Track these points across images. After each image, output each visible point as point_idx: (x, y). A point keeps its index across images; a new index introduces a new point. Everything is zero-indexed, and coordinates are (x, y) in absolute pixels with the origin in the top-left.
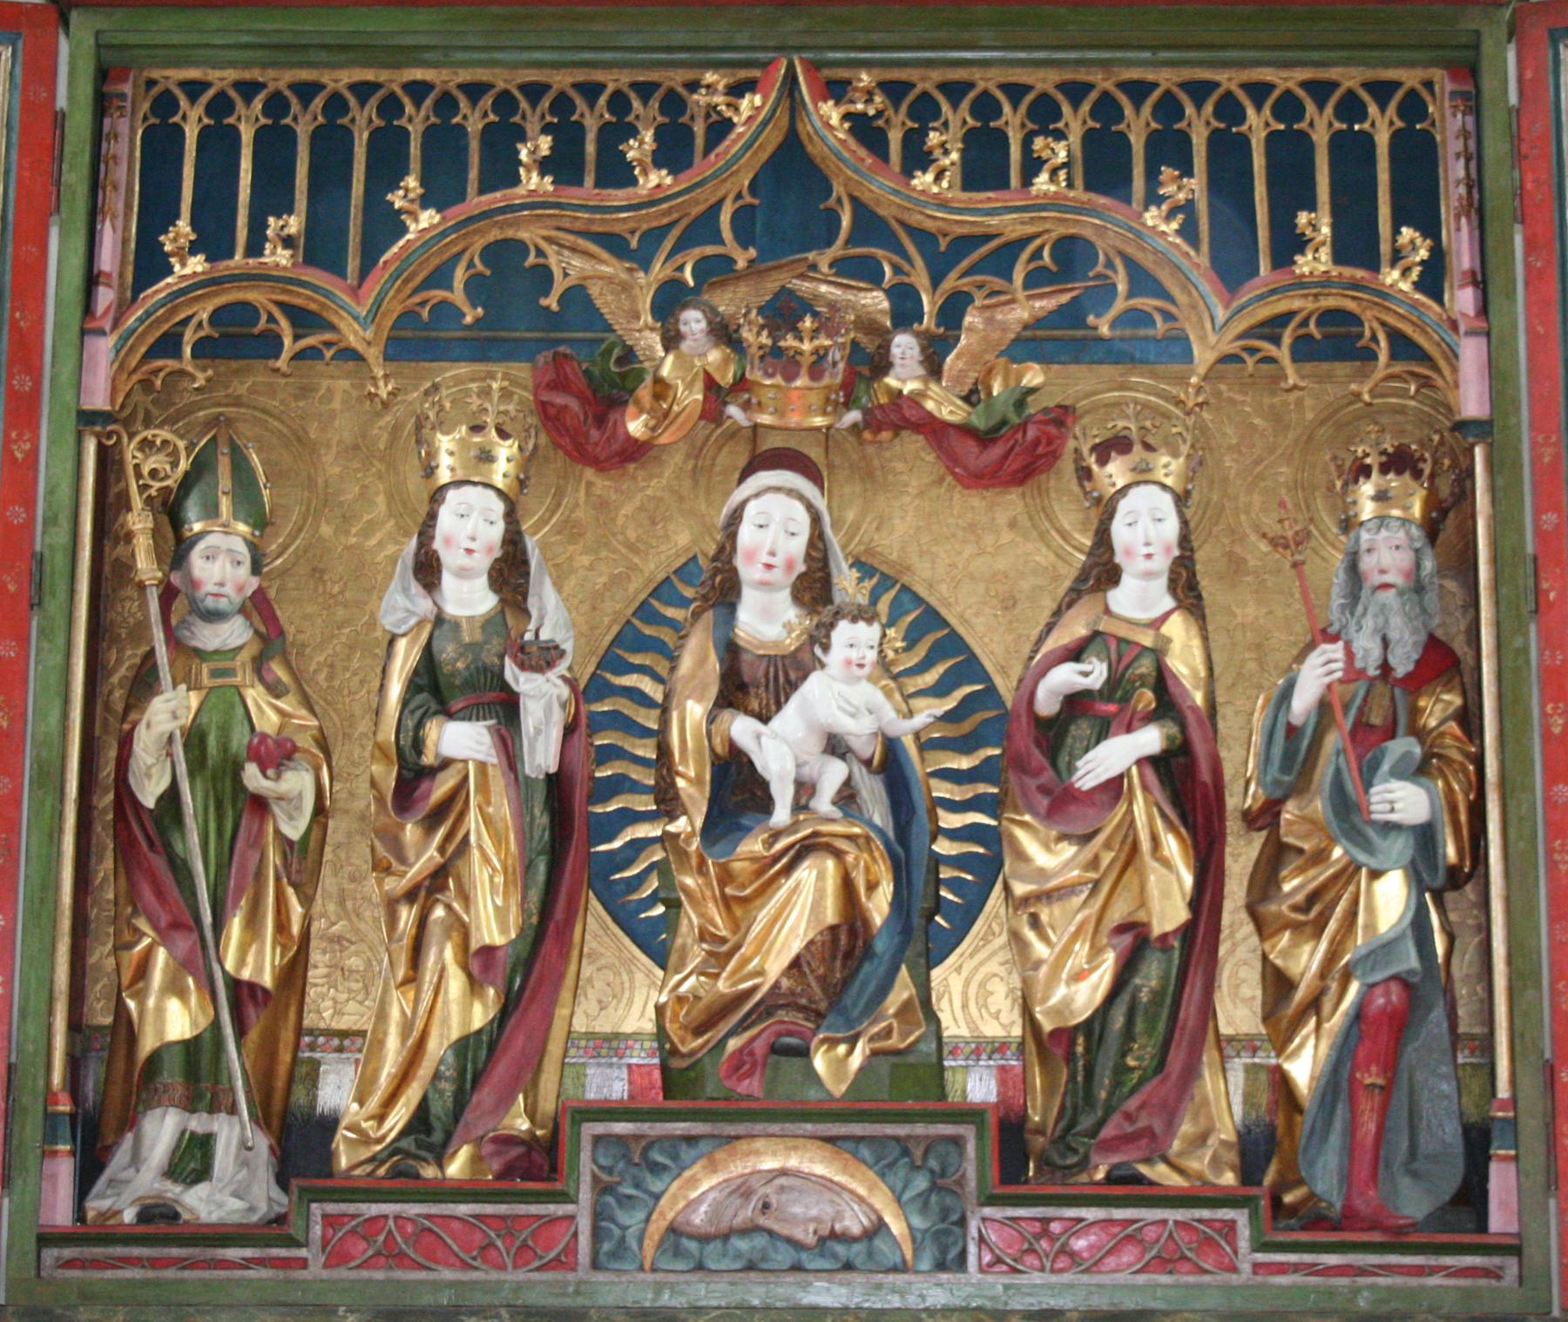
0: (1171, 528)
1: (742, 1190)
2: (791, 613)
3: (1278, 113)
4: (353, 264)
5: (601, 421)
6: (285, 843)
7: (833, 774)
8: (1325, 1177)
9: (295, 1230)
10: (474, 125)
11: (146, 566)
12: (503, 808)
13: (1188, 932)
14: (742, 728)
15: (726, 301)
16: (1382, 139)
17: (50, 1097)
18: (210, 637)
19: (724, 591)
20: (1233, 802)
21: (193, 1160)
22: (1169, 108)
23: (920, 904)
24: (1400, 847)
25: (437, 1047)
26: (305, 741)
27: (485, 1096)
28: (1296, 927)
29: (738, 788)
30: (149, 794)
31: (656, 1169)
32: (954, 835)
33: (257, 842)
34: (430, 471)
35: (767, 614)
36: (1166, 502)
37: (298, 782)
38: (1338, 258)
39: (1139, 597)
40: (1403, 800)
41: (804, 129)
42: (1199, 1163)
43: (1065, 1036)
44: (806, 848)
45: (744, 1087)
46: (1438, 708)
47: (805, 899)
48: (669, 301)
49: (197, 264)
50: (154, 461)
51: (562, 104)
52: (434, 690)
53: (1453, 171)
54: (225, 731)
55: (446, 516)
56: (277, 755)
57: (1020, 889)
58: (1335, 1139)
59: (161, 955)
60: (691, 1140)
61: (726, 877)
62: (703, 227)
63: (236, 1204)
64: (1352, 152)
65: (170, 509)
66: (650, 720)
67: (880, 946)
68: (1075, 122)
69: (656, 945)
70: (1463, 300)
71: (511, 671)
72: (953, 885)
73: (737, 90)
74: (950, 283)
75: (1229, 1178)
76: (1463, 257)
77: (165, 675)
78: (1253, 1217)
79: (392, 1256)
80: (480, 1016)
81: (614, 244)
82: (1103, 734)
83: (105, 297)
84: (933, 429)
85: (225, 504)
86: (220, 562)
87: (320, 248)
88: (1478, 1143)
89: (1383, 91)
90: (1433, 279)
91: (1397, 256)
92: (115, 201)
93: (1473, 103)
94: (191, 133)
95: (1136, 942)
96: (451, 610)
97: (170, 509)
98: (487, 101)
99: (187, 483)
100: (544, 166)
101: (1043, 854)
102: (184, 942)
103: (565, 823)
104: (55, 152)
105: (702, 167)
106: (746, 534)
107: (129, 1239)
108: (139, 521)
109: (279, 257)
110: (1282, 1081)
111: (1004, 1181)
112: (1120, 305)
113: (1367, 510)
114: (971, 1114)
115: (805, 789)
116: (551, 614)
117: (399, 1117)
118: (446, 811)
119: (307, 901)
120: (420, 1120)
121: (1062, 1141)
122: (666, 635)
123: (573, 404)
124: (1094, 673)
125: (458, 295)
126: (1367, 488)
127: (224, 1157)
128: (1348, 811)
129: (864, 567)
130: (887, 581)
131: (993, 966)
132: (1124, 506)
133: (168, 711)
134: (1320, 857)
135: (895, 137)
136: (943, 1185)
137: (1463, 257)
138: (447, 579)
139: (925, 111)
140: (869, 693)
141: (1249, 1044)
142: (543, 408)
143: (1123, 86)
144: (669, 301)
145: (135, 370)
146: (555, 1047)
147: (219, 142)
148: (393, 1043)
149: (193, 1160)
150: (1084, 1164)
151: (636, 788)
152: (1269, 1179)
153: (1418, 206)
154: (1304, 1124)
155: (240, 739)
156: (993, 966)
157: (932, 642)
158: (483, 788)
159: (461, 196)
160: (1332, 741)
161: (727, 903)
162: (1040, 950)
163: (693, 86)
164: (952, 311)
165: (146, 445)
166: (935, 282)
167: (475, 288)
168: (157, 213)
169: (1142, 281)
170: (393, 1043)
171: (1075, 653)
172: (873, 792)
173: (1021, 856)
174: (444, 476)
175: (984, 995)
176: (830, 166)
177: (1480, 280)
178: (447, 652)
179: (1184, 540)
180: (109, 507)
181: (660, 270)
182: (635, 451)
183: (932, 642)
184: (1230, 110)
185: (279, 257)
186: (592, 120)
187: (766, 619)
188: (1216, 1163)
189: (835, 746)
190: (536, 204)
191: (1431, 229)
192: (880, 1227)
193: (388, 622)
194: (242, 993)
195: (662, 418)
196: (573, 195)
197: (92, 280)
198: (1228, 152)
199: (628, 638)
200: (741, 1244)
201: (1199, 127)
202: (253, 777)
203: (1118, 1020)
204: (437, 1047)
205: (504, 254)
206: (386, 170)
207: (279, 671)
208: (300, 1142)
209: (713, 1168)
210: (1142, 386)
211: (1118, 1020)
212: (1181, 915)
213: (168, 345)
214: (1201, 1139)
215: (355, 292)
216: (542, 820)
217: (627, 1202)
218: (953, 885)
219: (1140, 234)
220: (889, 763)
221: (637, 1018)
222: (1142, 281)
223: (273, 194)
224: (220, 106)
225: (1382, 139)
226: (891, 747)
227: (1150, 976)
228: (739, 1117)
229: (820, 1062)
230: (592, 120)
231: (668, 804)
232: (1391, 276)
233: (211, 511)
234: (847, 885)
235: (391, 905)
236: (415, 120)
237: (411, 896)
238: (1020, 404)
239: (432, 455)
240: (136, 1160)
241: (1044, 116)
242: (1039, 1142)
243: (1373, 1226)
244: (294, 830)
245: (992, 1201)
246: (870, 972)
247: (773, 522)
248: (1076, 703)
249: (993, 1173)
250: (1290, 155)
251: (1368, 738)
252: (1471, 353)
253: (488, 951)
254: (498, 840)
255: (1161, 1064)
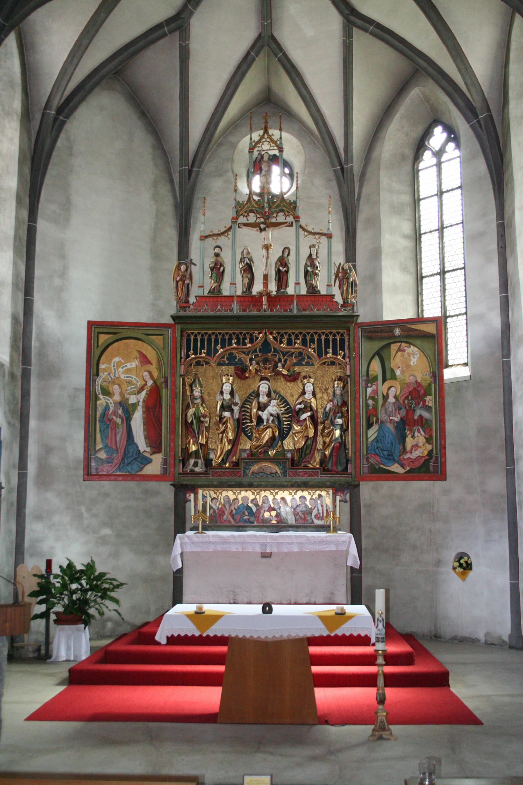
0: (312, 388)
1: (261, 468)
2: (266, 398)
3: (326, 336)
4: (212, 356)
5: (243, 374)
6: (206, 427)
7: (271, 418)
8: (329, 466)
9: (208, 472)
10: (227, 338)
11: (188, 393)
12: (232, 422)
13: (314, 437)
14: (260, 413)
15: (257, 359)
16: (338, 339)
17: (179, 457)
18: (196, 401)
19: (258, 395)
20: (319, 420)
21: (196, 464)
22: (312, 336)
23: (282, 433)
24: (339, 427)
25: (224, 451)
26: (208, 414)
27: (230, 457)
28: (326, 436)
29: (260, 420)
30: (190, 421)
31: (251, 465)
32: (286, 425)
33: (203, 427)
34: (222, 381)
35: (263, 398)
36: (311, 385)
37: (207, 419)
38: (333, 354)
39: (308, 396)
40: (339, 421)
41: (267, 338)
42: (315, 464)
43: (299, 449)
44: (269, 427)
45: (261, 456)
46: (344, 409)
47: (268, 433)
48: (251, 360)
49: (193, 356)
50: (188, 381)
51: (238, 335)
52: (223, 408)
53: (347, 344)
54: (198, 414)
55: (224, 387)
56: (204, 416)
57: (294, 432)
58: (331, 461)
59: (192, 440)
60: (255, 462)
61: (258, 431)
62: (255, 351)
63: (201, 470)
64: (335, 341)
65: (191, 386)
66: (249, 411)
67: (277, 439)
68: (301, 337)
69: (250, 438)
70: (347, 360)
71: (232, 406)
72: (286, 431)
73: (259, 333)
74: (285, 357)
75: (318, 466)
76: (347, 355)
77: (191, 407)
78: (321, 471)
79: (220, 475)
80: (229, 447)
81: (244, 353)
82: (304, 413)
83: (183, 360)
84: (283, 375)
85: (198, 386)
86: (197, 393)
87: (208, 354)
88: (347, 461)
89: (338, 333)
90: (344, 358)
91: (340, 354)
92: (183, 348)
93: (349, 335)
94: (192, 339)
95: (307, 438)
96: (225, 398)
97: (191, 386)
98: (228, 335)
99: (193, 383)
100: (236, 343)
101: (297, 428)
102: (194, 439)
103: (240, 427)
104: (176, 342)
105: (255, 343)
106: (261, 389)
107: (189, 474)
108: (187, 387)
109: (204, 355)
110: (325, 454)
111: (292, 466)
112: (306, 360)
113: (336, 385)
114: (288, 459)
115: (268, 420)
116: (237, 399)
117: (220, 460)
118: (226, 423)
119: (208, 433)
120: (223, 460)
121: (298, 462)
122: (251, 400)
123: (239, 372)
124: (302, 406)
125: (225, 359)
126: (336, 383)
127: (199, 464)
128: (333, 423)
129: (275, 392)
130: (278, 393)
131: (291, 441)
132: (306, 385)
133: (191, 411)
134: (329, 428)
135: (278, 339)
136: (284, 467)
137: (347, 355)
138: (224, 394)
139: (282, 336)
140: (275, 408)
141: (321, 449)
142: (236, 373)
143: (307, 333)
144: (251, 360)
145: (219, 457)
146: (238, 451)
147: (196, 340)
148: (219, 450)
149: (196, 464)
150: (301, 465)
151: (247, 419)
152: (323, 466)
153: (342, 348)
154: (327, 459)
155: (200, 414)
156: (291, 441)
157: (283, 400)
158: (229, 420)
159: (225, 347)
160: (331, 414)
161: (259, 434)
162: (296, 439)
163: (254, 333)
164: (286, 361)
165: (188, 378)
166: (284, 357)
167: (227, 359)
168: (188, 350)
169: (309, 357)
170: (219, 450)
171: (300, 403)
172: (276, 420)
173: (294, 428)
174: (224, 382)
175: (289, 444)
176: (271, 343)
177: (349, 357)
178: (225, 403)
179: (314, 389)
180: (184, 384)
181: (250, 356)
182: (247, 378)
183: (283, 400)
184: (320, 336)
185: (204, 355)
186: (241, 337)
187: (263, 399)
188: (317, 464)
189: (271, 415)
190: (235, 348)
191: (344, 351)
192: (277, 472)
193: (217, 399)
194: (201, 445)
195: (250, 374)
196: (239, 347)
197: (181, 358)
198: (319, 341)
199: (246, 401)
200: (261, 474)
201: (316, 338)
202: (202, 419)
203: (305, 448)
204: (224, 451)
205: (231, 354)
206: (216, 343)
207: (204, 405)
208: (208, 462)
209: (257, 465)
210: (309, 369)
211: (305, 448)
212: (313, 435)
213: (191, 365)
214: (315, 461)
215: (213, 359)
216: (236, 423)
217: (248, 469)
218: (286, 431)
219: (308, 352)
220: (278, 417)
221: (248, 447)
222: (309, 357)
223: (202, 347)
224: (196, 336)
225: (338, 339)
226: (278, 414)
227: (309, 442)
228: (259, 460)
229: (270, 453)
230: (241, 337)
231: (251, 421)
232: (339, 357)
233: (196, 386)
234: (273, 432)
235: (219, 434)
236: (220, 337)
237: (221, 433)
238: (294, 372)
239: (222, 379)
240: (189, 465)
241: (297, 337)
242: (296, 462)
243: (335, 471)
244: (207, 425)
245: (290, 469)
246: (276, 442)
247: (264, 387)
248: (300, 409)
249: (290, 465)
250: (327, 341)
251: (335, 414)
252: (348, 366)
253: (230, 440)
254: (231, 426)
255: (310, 452)
